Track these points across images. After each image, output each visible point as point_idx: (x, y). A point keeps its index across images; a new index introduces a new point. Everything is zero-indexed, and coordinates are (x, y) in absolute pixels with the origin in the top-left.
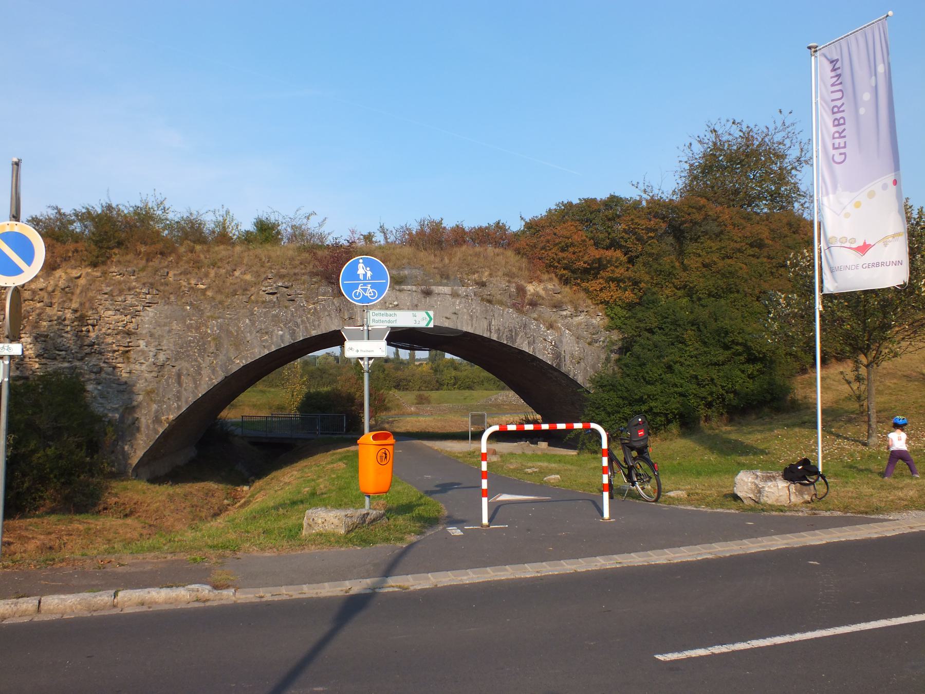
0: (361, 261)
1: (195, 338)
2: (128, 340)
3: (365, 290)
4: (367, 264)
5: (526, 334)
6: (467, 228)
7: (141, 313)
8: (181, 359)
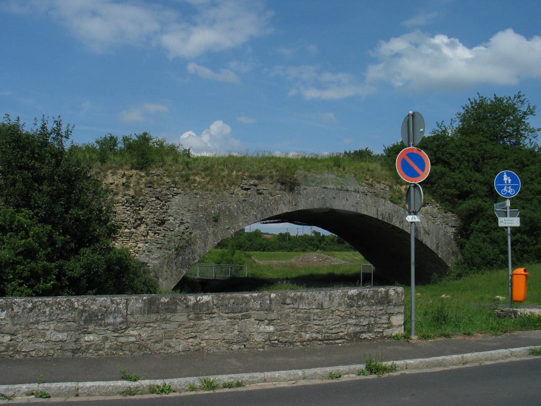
0: (505, 173)
1: (204, 215)
2: (163, 216)
3: (508, 189)
4: (509, 175)
5: (398, 216)
6: (383, 153)
7: (171, 200)
8: (196, 228)
